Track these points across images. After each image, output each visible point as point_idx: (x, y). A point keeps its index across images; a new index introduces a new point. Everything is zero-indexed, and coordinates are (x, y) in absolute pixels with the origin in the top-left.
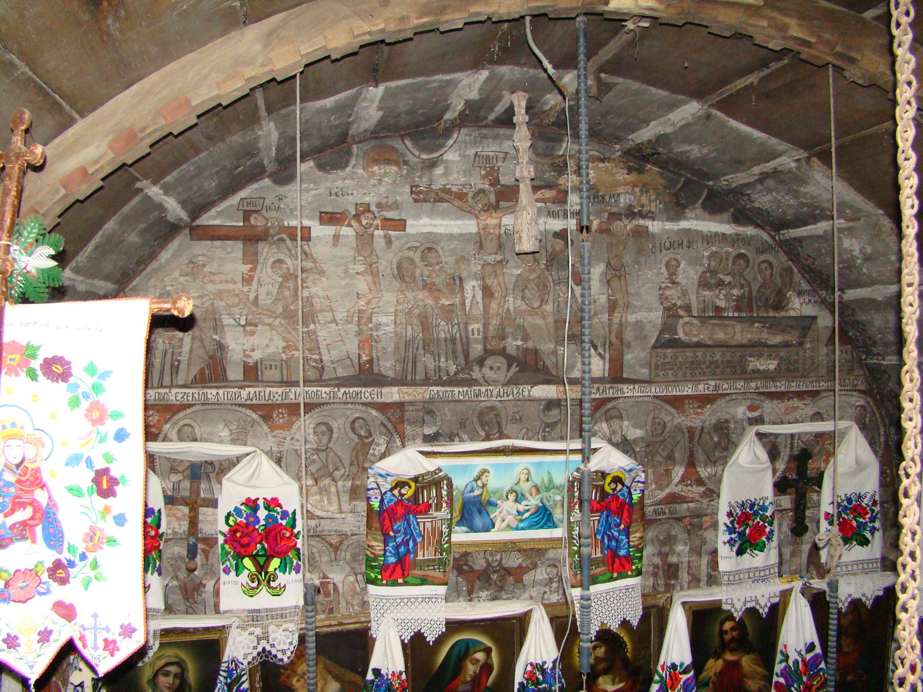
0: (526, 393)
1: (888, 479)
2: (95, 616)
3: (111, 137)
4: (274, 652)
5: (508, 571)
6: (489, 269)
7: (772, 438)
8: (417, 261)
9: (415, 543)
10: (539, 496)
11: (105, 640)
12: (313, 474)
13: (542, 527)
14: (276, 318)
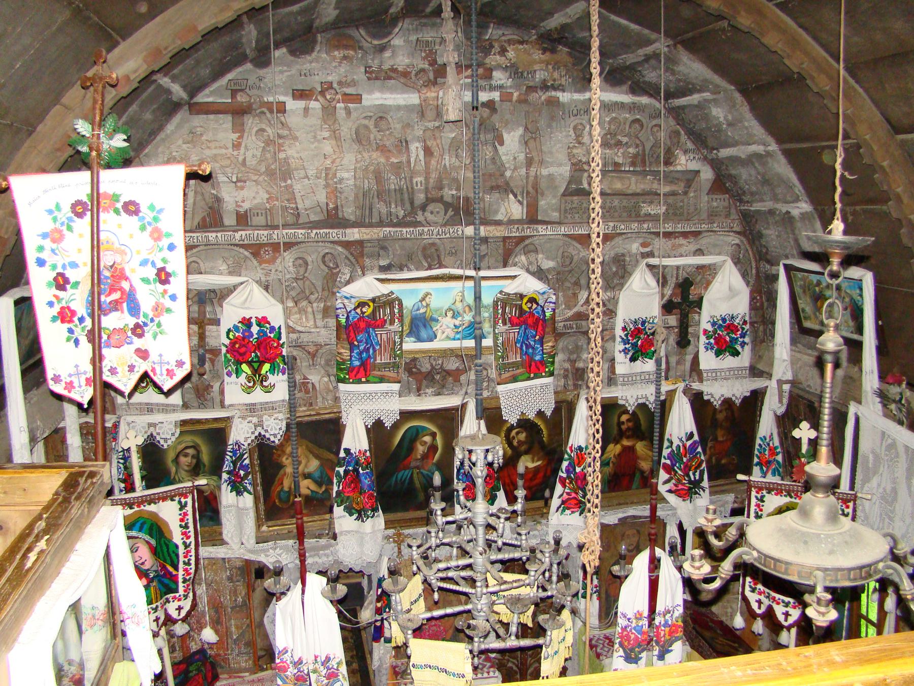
0: (460, 233)
2: (161, 355)
3: (144, 53)
4: (267, 436)
5: (448, 373)
6: (429, 133)
8: (372, 127)
9: (375, 351)
11: (167, 370)
14: (260, 175)
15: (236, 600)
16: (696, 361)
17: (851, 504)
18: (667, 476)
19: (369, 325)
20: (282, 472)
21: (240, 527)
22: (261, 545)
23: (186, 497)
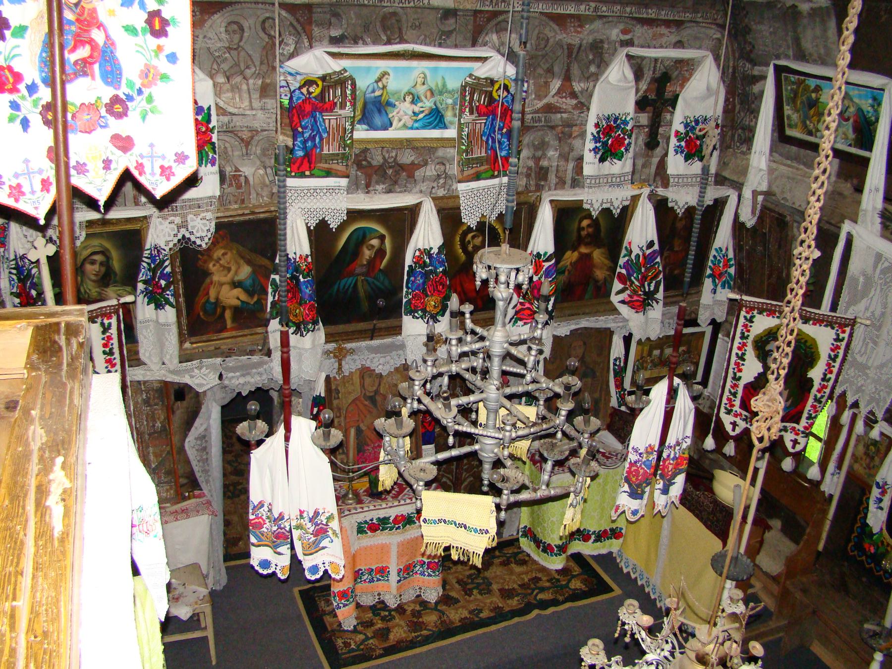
2: (152, 146)
4: (193, 239)
5: (402, 167)
7: (639, 61)
9: (321, 139)
10: (433, 100)
11: (162, 167)
12: (225, 72)
13: (434, 128)
15: (154, 426)
16: (662, 165)
17: (848, 329)
18: (621, 286)
19: (315, 108)
20: (208, 281)
21: (161, 345)
22: (185, 364)
23: (110, 317)
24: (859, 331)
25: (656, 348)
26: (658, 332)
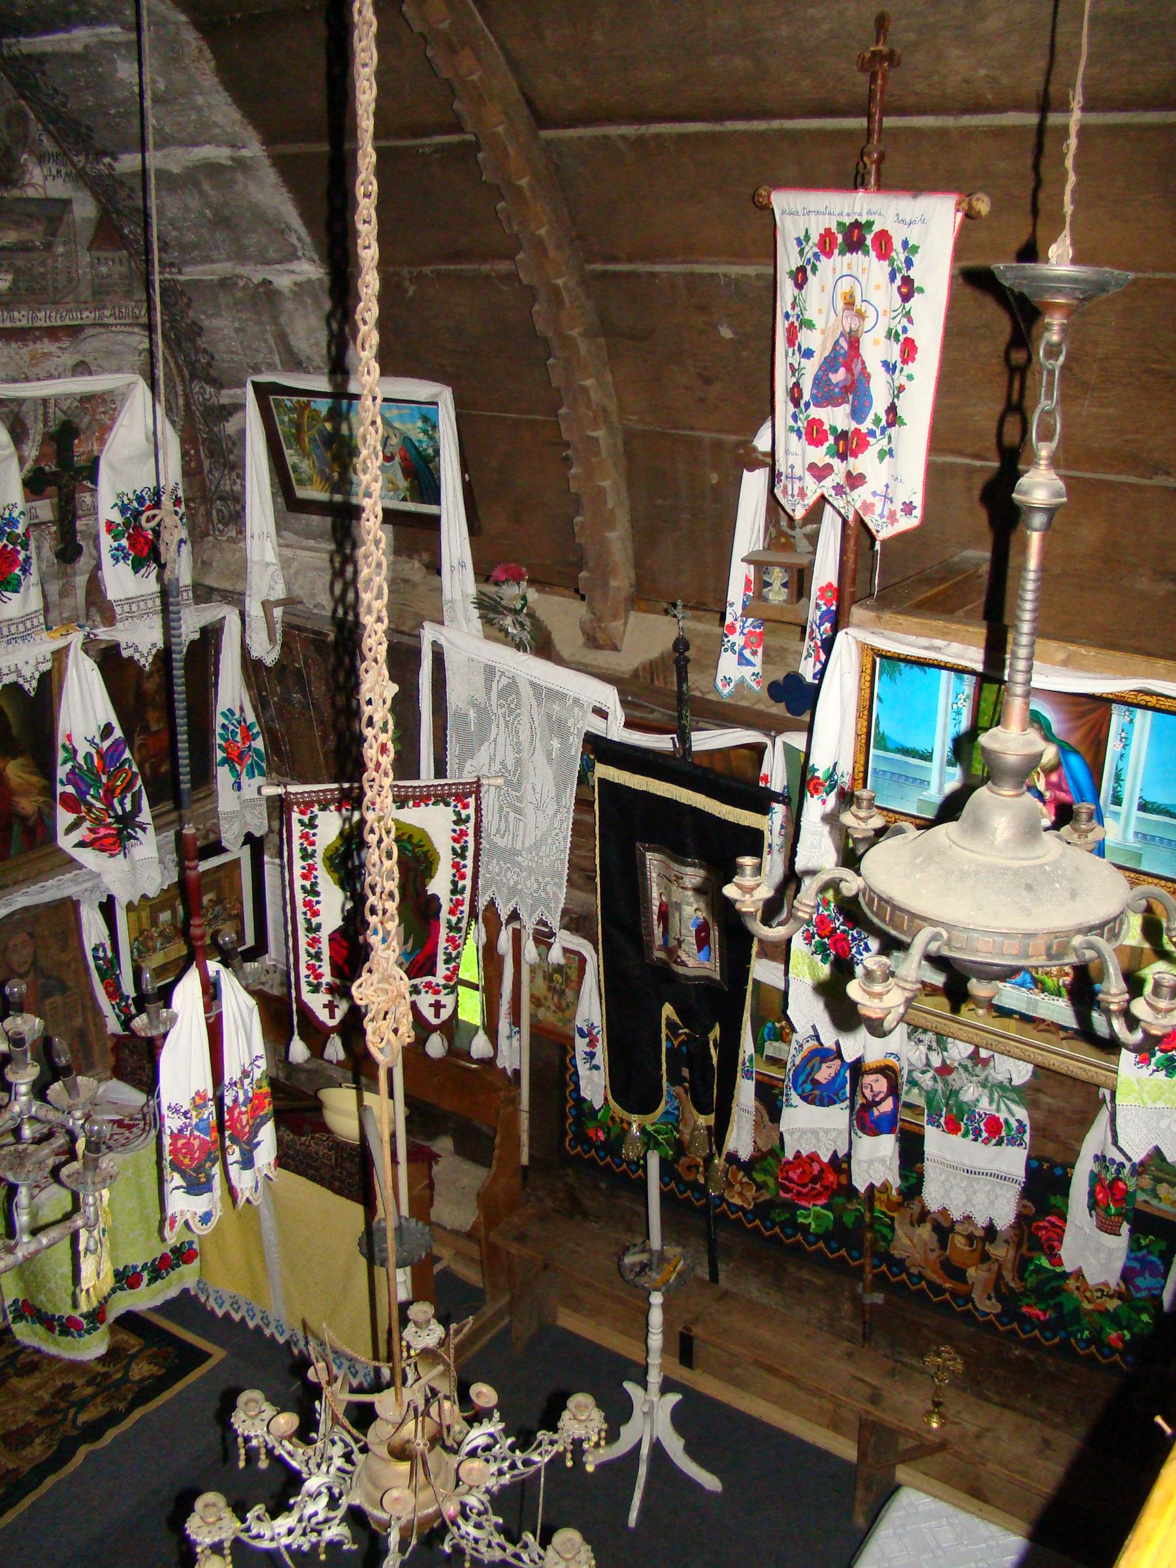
1: (193, 464)
7: (13, 406)
16: (95, 586)
17: (471, 801)
18: (71, 817)
24: (489, 800)
25: (162, 910)
26: (159, 880)
